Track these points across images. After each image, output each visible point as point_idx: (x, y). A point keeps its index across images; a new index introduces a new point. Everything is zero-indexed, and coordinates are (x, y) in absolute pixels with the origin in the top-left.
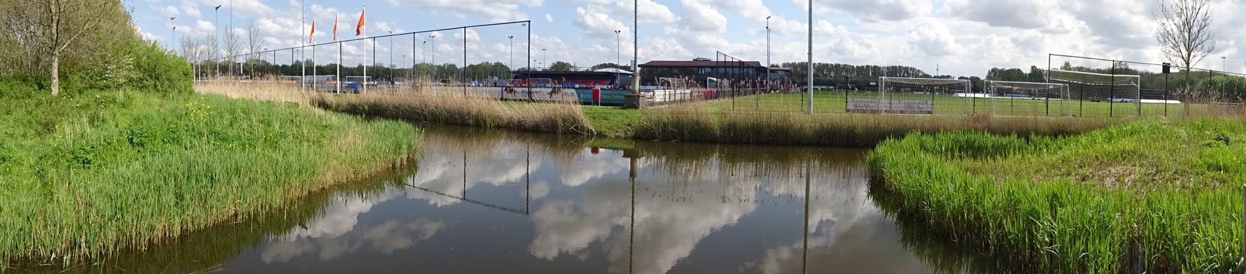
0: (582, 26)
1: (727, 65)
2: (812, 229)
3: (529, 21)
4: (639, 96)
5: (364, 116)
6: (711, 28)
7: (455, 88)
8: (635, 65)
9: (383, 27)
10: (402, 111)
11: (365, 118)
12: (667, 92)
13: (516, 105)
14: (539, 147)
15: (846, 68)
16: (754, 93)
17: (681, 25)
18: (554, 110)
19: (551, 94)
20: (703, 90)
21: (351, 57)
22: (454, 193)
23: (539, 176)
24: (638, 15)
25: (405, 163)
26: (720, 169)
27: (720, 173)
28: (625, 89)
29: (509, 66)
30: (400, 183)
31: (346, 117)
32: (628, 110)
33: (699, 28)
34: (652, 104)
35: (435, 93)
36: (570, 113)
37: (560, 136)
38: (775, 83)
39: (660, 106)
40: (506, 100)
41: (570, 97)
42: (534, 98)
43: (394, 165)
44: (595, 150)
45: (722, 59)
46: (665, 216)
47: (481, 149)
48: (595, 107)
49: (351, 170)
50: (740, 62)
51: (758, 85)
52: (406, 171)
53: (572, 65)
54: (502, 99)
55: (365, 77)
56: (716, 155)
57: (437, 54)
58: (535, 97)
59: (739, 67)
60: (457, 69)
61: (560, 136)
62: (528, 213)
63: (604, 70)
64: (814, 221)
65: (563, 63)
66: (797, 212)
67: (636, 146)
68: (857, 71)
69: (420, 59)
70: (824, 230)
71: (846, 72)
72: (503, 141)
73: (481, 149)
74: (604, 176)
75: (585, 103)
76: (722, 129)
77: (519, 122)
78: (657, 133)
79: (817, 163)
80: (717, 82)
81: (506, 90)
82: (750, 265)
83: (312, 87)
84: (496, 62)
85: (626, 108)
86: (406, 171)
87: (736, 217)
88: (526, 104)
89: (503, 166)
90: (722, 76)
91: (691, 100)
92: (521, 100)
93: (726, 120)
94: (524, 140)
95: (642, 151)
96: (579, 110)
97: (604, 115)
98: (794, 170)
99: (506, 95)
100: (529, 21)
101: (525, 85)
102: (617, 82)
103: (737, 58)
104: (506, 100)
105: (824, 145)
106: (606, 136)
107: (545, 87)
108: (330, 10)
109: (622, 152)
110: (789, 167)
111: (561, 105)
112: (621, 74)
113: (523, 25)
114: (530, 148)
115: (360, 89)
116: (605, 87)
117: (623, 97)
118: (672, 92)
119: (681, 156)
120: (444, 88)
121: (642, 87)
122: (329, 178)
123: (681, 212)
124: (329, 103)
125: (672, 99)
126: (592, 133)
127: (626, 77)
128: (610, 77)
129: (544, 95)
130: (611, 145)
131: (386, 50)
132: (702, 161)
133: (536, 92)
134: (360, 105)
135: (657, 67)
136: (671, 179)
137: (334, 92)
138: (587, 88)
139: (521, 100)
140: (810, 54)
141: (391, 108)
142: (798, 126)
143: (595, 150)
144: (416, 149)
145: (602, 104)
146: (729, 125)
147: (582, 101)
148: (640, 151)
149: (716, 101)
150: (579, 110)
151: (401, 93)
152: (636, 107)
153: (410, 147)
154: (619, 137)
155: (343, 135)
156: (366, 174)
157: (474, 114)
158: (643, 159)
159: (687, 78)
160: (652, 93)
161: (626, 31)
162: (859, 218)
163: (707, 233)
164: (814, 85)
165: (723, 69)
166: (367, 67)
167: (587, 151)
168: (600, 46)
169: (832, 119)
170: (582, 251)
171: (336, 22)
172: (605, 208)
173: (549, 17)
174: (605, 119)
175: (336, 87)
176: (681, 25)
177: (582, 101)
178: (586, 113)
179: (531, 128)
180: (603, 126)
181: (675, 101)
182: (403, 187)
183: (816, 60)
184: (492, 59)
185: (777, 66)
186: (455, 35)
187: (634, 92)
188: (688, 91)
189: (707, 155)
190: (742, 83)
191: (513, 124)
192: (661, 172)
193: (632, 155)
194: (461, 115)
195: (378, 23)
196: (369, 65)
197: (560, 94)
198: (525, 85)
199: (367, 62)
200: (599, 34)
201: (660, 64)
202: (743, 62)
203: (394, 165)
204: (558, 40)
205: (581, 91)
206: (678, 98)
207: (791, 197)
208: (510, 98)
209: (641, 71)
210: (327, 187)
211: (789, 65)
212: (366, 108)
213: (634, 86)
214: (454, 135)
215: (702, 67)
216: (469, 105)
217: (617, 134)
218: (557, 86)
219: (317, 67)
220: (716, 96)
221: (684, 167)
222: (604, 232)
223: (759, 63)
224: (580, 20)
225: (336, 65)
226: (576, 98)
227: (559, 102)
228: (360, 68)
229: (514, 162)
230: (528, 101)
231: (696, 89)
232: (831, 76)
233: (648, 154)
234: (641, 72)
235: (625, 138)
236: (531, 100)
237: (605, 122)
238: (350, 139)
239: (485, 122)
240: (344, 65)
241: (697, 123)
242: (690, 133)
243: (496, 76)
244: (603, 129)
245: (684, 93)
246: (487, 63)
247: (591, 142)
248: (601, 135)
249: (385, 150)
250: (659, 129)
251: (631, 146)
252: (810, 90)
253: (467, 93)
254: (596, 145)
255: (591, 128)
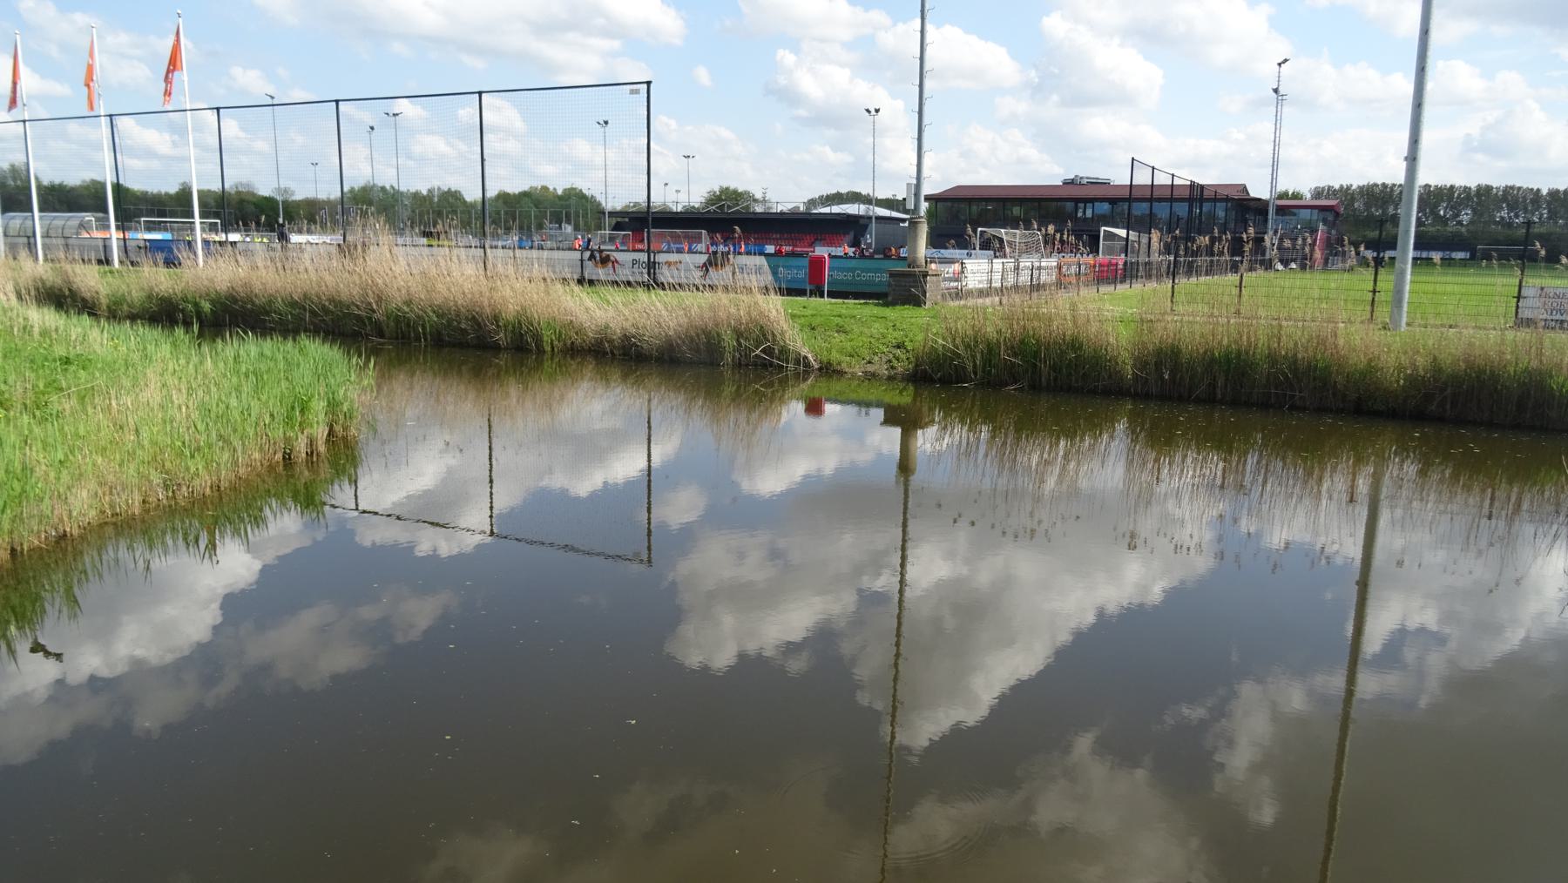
0: (789, 96)
1: (1156, 194)
2: (1374, 640)
3: (649, 83)
4: (925, 275)
5: (196, 328)
6: (1116, 98)
7: (455, 251)
8: (917, 195)
9: (252, 82)
10: (313, 313)
11: (201, 335)
12: (998, 263)
13: (617, 297)
14: (678, 399)
15: (1513, 198)
16: (1235, 268)
17: (1038, 90)
18: (712, 308)
19: (705, 267)
20: (1090, 259)
21: (155, 164)
22: (475, 520)
23: (677, 472)
24: (927, 67)
25: (322, 448)
26: (1130, 463)
27: (1128, 470)
28: (887, 257)
29: (600, 198)
30: (309, 500)
31: (150, 335)
32: (898, 307)
33: (1081, 100)
34: (958, 294)
35: (403, 262)
36: (754, 314)
37: (728, 374)
38: (1300, 241)
39: (980, 301)
40: (591, 282)
41: (753, 277)
42: (661, 279)
43: (288, 459)
44: (814, 408)
45: (1142, 178)
46: (985, 576)
47: (529, 404)
48: (815, 301)
49: (156, 479)
50: (1193, 185)
51: (1247, 248)
52: (325, 470)
53: (758, 196)
54: (580, 282)
55: (197, 220)
56: (1121, 426)
57: (411, 163)
58: (665, 275)
59: (1190, 200)
60: (465, 202)
61: (728, 374)
62: (649, 561)
63: (836, 209)
64: (1381, 624)
65: (735, 192)
66: (1329, 596)
67: (914, 400)
68: (1549, 204)
69: (360, 173)
70: (1410, 655)
71: (1511, 208)
72: (585, 385)
73: (529, 404)
74: (838, 471)
75: (792, 291)
76: (1141, 362)
77: (626, 337)
78: (970, 368)
79: (1411, 469)
80: (1127, 238)
81: (592, 257)
82: (1193, 713)
83: (31, 247)
84: (568, 186)
85: (893, 304)
86: (325, 470)
87: (1156, 593)
88: (642, 294)
89: (591, 448)
90: (1144, 224)
91: (1060, 284)
92: (629, 283)
93: (1154, 340)
94: (638, 383)
95: (931, 410)
96: (775, 308)
97: (837, 320)
98: (1335, 483)
99: (592, 271)
100: (649, 83)
101: (640, 246)
102: (870, 238)
103: (1185, 176)
104: (591, 282)
105: (1440, 420)
106: (841, 373)
107: (690, 251)
108: (80, 18)
109: (878, 414)
110: (1322, 470)
111: (732, 295)
112: (879, 218)
113: (633, 92)
114: (655, 402)
115: (183, 255)
116: (839, 251)
117: (885, 277)
118: (1010, 263)
119: (1027, 426)
120: (427, 250)
121: (934, 252)
122: (82, 505)
123: (1025, 564)
124: (87, 295)
125: (1011, 280)
126: (807, 364)
127: (889, 227)
128: (851, 227)
129: (688, 270)
130: (853, 396)
131: (263, 146)
132: (1082, 440)
133: (669, 264)
134: (185, 299)
135: (970, 201)
136: (1002, 482)
137: (100, 262)
138: (793, 254)
139: (629, 283)
140: (1412, 159)
141: (279, 304)
142: (1358, 360)
143: (814, 408)
144: (351, 410)
145: (832, 295)
146: (1159, 352)
147: (783, 286)
148: (925, 409)
149: (1122, 288)
150: (775, 308)
151: (308, 263)
152: (917, 301)
153: (333, 405)
154: (874, 375)
155: (126, 383)
156: (203, 483)
157: (511, 318)
158: (932, 431)
159: (1051, 228)
160: (957, 267)
161: (897, 111)
162: (1526, 639)
163: (1090, 618)
164: (1416, 248)
165: (1145, 205)
166: (199, 192)
167: (795, 409)
168: (827, 149)
169: (1471, 345)
170: (791, 648)
171: (91, 55)
172: (847, 544)
173: (703, 75)
174: (841, 330)
175: (106, 248)
176: (1038, 90)
177: (783, 286)
178: (793, 316)
179: (655, 353)
180: (835, 348)
181: (1016, 288)
182: (320, 513)
183: (1432, 174)
184: (557, 180)
185: (1296, 196)
186: (461, 112)
187: (912, 263)
188: (1052, 262)
189: (1097, 424)
190: (1204, 240)
191: (611, 341)
192: (976, 466)
193: (905, 420)
194: (476, 321)
195: (237, 71)
196: (206, 187)
197: (728, 269)
198: (640, 246)
199: (202, 178)
200: (828, 119)
201: (978, 194)
202: (1202, 187)
203: (288, 459)
204: (725, 133)
205: (781, 261)
206: (1024, 278)
207: (1316, 558)
208: (602, 277)
209: (929, 212)
210: (76, 532)
211: (1330, 192)
212: (206, 306)
213: (914, 250)
214: (460, 373)
215: (1086, 201)
216: (496, 296)
217: (870, 368)
218: (721, 248)
219: (201, 194)
220: (1129, 273)
221: (1032, 456)
222: (839, 605)
223: (1244, 189)
224: (782, 81)
225: (103, 185)
226: (768, 278)
227: (726, 289)
228: (183, 197)
229: (614, 441)
230: (648, 286)
231: (1069, 258)
232: (1460, 223)
233: (945, 418)
234: (931, 214)
235: (890, 378)
236: (654, 284)
237: (838, 338)
238: (152, 395)
239: (538, 338)
240: (134, 184)
241: (1075, 344)
242: (1054, 368)
243: (568, 222)
244: (835, 356)
245: (1039, 268)
246: (545, 188)
247: (804, 386)
248: (828, 371)
249: (260, 416)
250: (974, 357)
251: (904, 397)
252: (1405, 263)
253: (489, 266)
254: (816, 394)
255: (805, 351)
